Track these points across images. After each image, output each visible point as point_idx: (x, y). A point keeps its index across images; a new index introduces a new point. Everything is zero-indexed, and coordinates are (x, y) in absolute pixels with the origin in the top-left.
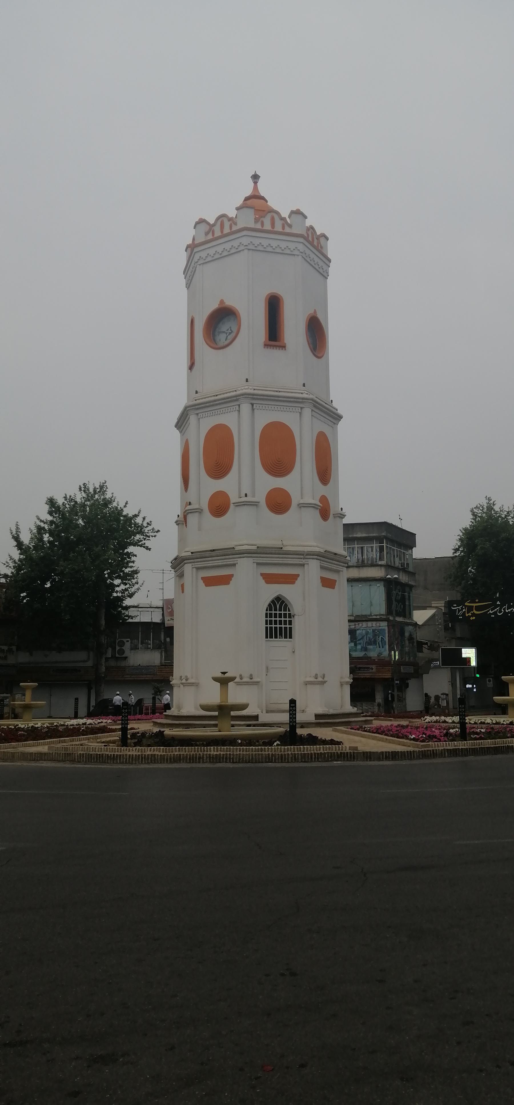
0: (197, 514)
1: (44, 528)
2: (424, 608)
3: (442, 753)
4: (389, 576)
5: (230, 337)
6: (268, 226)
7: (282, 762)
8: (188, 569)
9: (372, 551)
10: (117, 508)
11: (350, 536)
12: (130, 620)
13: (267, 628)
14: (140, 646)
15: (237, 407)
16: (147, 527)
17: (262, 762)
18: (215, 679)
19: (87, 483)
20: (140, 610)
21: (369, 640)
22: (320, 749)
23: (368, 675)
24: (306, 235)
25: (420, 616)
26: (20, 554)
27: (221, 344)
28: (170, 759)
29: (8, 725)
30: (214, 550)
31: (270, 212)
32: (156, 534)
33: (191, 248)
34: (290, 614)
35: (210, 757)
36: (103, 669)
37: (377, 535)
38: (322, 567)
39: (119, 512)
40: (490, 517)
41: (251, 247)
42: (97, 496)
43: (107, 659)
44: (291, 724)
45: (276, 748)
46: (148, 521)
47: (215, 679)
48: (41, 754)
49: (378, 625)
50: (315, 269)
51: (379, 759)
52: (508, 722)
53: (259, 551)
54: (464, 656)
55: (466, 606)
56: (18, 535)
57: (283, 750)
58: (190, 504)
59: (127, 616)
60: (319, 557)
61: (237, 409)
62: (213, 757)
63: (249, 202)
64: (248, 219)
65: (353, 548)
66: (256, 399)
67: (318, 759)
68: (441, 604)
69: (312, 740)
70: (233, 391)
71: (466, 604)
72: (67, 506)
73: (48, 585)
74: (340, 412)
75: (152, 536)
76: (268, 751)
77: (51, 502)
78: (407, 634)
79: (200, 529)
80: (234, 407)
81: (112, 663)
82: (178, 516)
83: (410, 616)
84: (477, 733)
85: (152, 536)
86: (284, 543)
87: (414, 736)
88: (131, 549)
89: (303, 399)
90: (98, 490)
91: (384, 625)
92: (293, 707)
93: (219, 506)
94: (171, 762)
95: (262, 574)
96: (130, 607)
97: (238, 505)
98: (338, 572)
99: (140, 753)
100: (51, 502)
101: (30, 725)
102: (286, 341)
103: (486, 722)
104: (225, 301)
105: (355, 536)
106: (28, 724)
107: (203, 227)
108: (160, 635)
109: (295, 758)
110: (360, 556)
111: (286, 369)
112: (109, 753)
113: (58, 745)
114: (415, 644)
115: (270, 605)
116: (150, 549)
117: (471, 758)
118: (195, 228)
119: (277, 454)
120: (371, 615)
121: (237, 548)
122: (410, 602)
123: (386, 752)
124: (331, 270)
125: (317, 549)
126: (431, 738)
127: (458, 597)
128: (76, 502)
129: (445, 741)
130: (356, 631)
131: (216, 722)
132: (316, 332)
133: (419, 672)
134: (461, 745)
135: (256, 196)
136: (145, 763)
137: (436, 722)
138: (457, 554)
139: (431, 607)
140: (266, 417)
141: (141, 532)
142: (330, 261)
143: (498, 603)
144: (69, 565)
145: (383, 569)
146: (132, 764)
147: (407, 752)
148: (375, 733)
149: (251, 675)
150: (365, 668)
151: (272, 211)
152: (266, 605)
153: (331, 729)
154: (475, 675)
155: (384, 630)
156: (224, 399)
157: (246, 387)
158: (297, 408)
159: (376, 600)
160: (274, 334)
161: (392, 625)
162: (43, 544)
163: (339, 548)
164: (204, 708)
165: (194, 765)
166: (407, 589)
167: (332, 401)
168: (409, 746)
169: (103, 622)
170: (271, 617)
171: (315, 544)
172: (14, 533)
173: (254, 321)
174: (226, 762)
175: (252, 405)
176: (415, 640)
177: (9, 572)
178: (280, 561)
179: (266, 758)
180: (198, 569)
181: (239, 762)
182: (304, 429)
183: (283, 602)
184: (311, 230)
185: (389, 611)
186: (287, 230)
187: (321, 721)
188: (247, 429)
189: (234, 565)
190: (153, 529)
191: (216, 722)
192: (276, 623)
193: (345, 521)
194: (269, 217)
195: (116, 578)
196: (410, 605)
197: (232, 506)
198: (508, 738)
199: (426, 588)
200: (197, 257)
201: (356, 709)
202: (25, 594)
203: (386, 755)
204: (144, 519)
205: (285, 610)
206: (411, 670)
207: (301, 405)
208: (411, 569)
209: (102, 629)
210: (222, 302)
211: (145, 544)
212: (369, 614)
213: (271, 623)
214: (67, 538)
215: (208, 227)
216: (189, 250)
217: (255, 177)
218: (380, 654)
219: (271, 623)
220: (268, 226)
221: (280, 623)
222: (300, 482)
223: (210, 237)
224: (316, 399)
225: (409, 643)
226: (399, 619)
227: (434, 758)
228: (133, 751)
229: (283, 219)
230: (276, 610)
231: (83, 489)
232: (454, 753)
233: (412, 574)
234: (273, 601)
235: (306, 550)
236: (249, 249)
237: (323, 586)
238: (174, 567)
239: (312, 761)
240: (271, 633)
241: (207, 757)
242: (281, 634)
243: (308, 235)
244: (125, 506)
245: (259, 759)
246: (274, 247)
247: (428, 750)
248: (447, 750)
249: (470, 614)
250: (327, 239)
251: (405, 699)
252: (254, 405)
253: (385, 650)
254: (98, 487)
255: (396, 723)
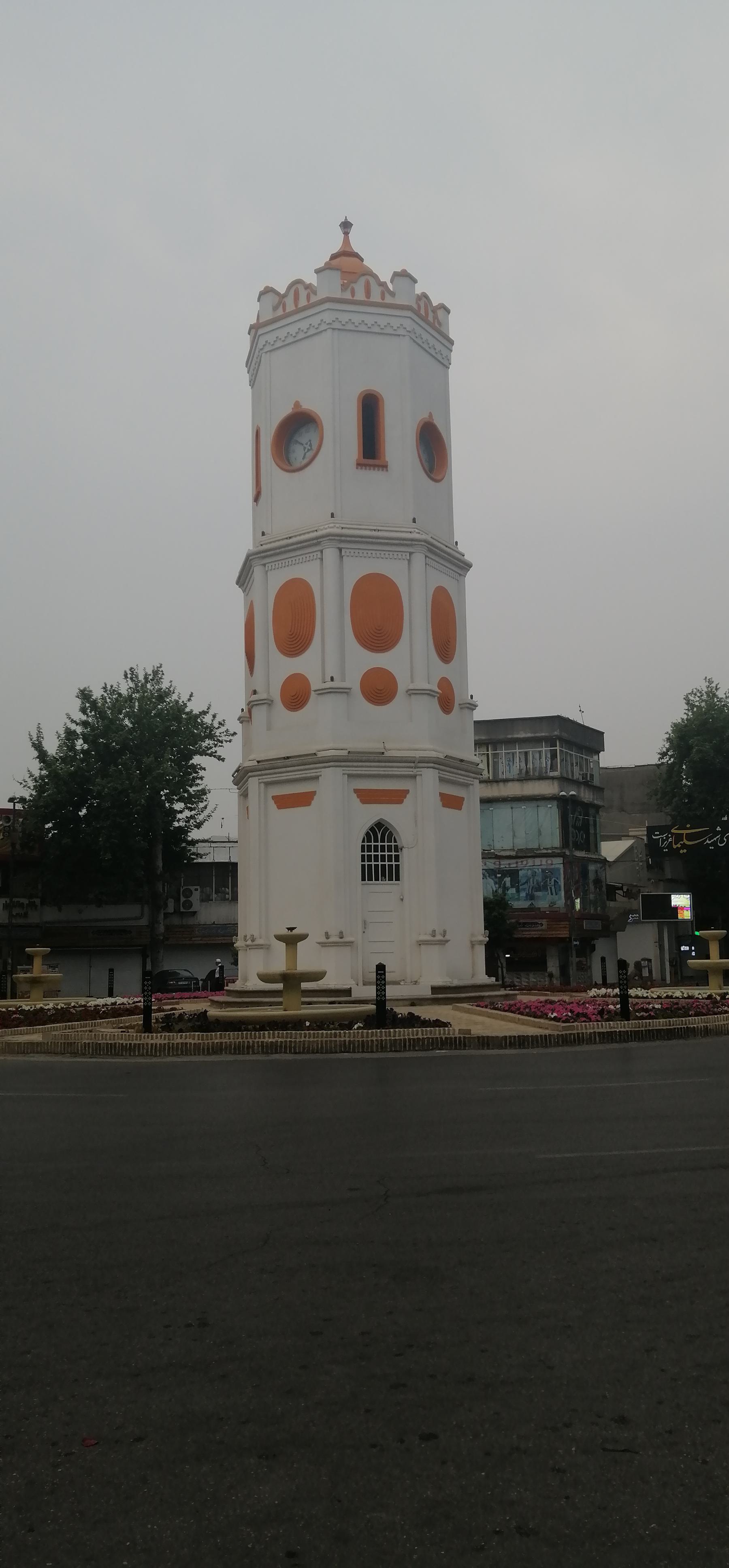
0: (265, 707)
1: (75, 731)
2: (618, 838)
3: (591, 1037)
4: (563, 793)
5: (310, 454)
6: (360, 295)
7: (363, 1052)
8: (253, 784)
9: (540, 757)
10: (177, 702)
11: (509, 736)
12: (200, 860)
13: (363, 866)
14: (214, 896)
15: (319, 553)
16: (219, 728)
17: (336, 1052)
18: (279, 938)
19: (135, 667)
20: (213, 845)
21: (538, 883)
22: (437, 1033)
23: (534, 934)
24: (415, 306)
25: (611, 850)
26: (41, 769)
27: (297, 464)
28: (208, 1049)
29: (7, 1007)
30: (288, 758)
31: (364, 275)
32: (231, 737)
33: (255, 329)
34: (396, 847)
35: (262, 1046)
36: (162, 929)
37: (547, 734)
38: (441, 780)
39: (179, 708)
40: (711, 706)
41: (336, 325)
42: (149, 686)
43: (166, 915)
44: (379, 998)
45: (357, 1033)
46: (220, 720)
47: (279, 938)
48: (32, 1044)
49: (549, 862)
50: (431, 355)
51: (500, 1047)
52: (705, 996)
53: (350, 758)
54: (673, 904)
55: (672, 834)
56: (40, 743)
57: (365, 1035)
58: (255, 692)
59: (193, 854)
60: (436, 766)
61: (319, 556)
62: (267, 1046)
63: (336, 262)
64: (332, 286)
65: (513, 754)
66: (345, 542)
67: (414, 1047)
68: (642, 832)
69: (412, 1021)
70: (313, 531)
71: (673, 831)
72: (108, 700)
73: (83, 812)
74: (467, 558)
75: (226, 741)
76: (345, 1036)
77: (85, 695)
78: (592, 876)
79: (269, 728)
80: (315, 554)
81: (176, 921)
82: (243, 710)
83: (597, 849)
84: (647, 1010)
85: (226, 741)
86: (388, 746)
87: (555, 1014)
88: (197, 760)
89: (412, 540)
90: (151, 677)
91: (558, 862)
92: (381, 975)
93: (296, 695)
94: (209, 1054)
95: (356, 791)
96: (198, 841)
97: (322, 692)
98: (466, 785)
99: (166, 1042)
100: (85, 695)
101: (38, 1007)
102: (387, 459)
103: (674, 995)
104: (301, 404)
105: (516, 736)
106: (35, 1005)
107: (270, 299)
108: (227, 872)
109: (382, 1047)
110: (523, 764)
111: (389, 497)
112: (125, 1043)
113: (57, 1031)
114: (604, 889)
115: (367, 834)
116: (223, 760)
117: (633, 1045)
118: (259, 301)
119: (377, 620)
120: (539, 849)
121: (320, 754)
122: (595, 829)
123: (510, 1037)
124: (454, 356)
125: (433, 754)
126: (577, 1017)
127: (666, 820)
128: (120, 695)
129: (598, 1021)
130: (518, 871)
131: (280, 1000)
132: (432, 445)
133: (610, 929)
134: (619, 1026)
135: (347, 253)
136: (173, 1055)
137: (605, 996)
138: (665, 761)
139: (628, 836)
140: (358, 567)
141: (211, 736)
142: (452, 342)
143: (719, 829)
144: (108, 783)
145: (556, 783)
146: (156, 1056)
147: (541, 1036)
148: (506, 1011)
149: (341, 933)
150: (532, 923)
151: (369, 273)
152: (362, 834)
153: (450, 1007)
154: (693, 932)
155: (558, 869)
156: (301, 542)
157: (332, 525)
158: (404, 554)
159: (544, 826)
160: (371, 449)
161: (569, 862)
162: (75, 755)
163: (468, 752)
164: (264, 978)
165: (240, 1057)
166: (592, 811)
167: (457, 543)
168: (547, 1028)
169: (160, 863)
170: (369, 850)
171: (431, 747)
172: (35, 739)
173: (341, 430)
174: (285, 1052)
175: (340, 550)
176: (604, 884)
177: (27, 794)
178: (381, 771)
179: (340, 1046)
180: (267, 784)
181: (303, 1053)
182: (415, 585)
183: (387, 829)
184: (424, 299)
185: (565, 843)
186: (389, 300)
187: (440, 996)
188: (331, 584)
189: (317, 778)
190: (227, 731)
191: (280, 1000)
192: (376, 860)
193: (479, 715)
194: (362, 281)
195: (178, 801)
196: (595, 834)
197: (313, 693)
198: (690, 1016)
199: (622, 810)
200: (262, 341)
201: (493, 979)
202: (50, 825)
203: (510, 1042)
204: (214, 716)
205: (390, 841)
206: (598, 925)
207: (411, 550)
208: (596, 782)
209: (159, 872)
210: (297, 404)
211: (216, 752)
212: (536, 846)
213: (369, 860)
214: (107, 746)
215: (277, 299)
216: (253, 331)
217: (346, 226)
218: (552, 904)
219: (369, 860)
220: (360, 295)
221: (383, 859)
222: (410, 659)
223: (280, 312)
224: (432, 540)
225: (596, 888)
226: (580, 854)
227: (579, 1044)
228: (158, 1039)
229: (383, 285)
230: (376, 841)
231: (129, 676)
232: (608, 1037)
233: (599, 790)
234: (372, 829)
235: (417, 756)
236: (334, 329)
237: (444, 805)
238: (236, 782)
239: (405, 1050)
240: (369, 874)
241: (258, 1046)
242: (384, 875)
243: (419, 307)
244: (189, 700)
245: (331, 1048)
246: (357, 324)
247: (571, 1034)
248: (599, 1033)
249: (679, 846)
250: (448, 311)
251: (590, 967)
252: (343, 551)
253: (560, 899)
254: (150, 672)
255: (543, 998)
